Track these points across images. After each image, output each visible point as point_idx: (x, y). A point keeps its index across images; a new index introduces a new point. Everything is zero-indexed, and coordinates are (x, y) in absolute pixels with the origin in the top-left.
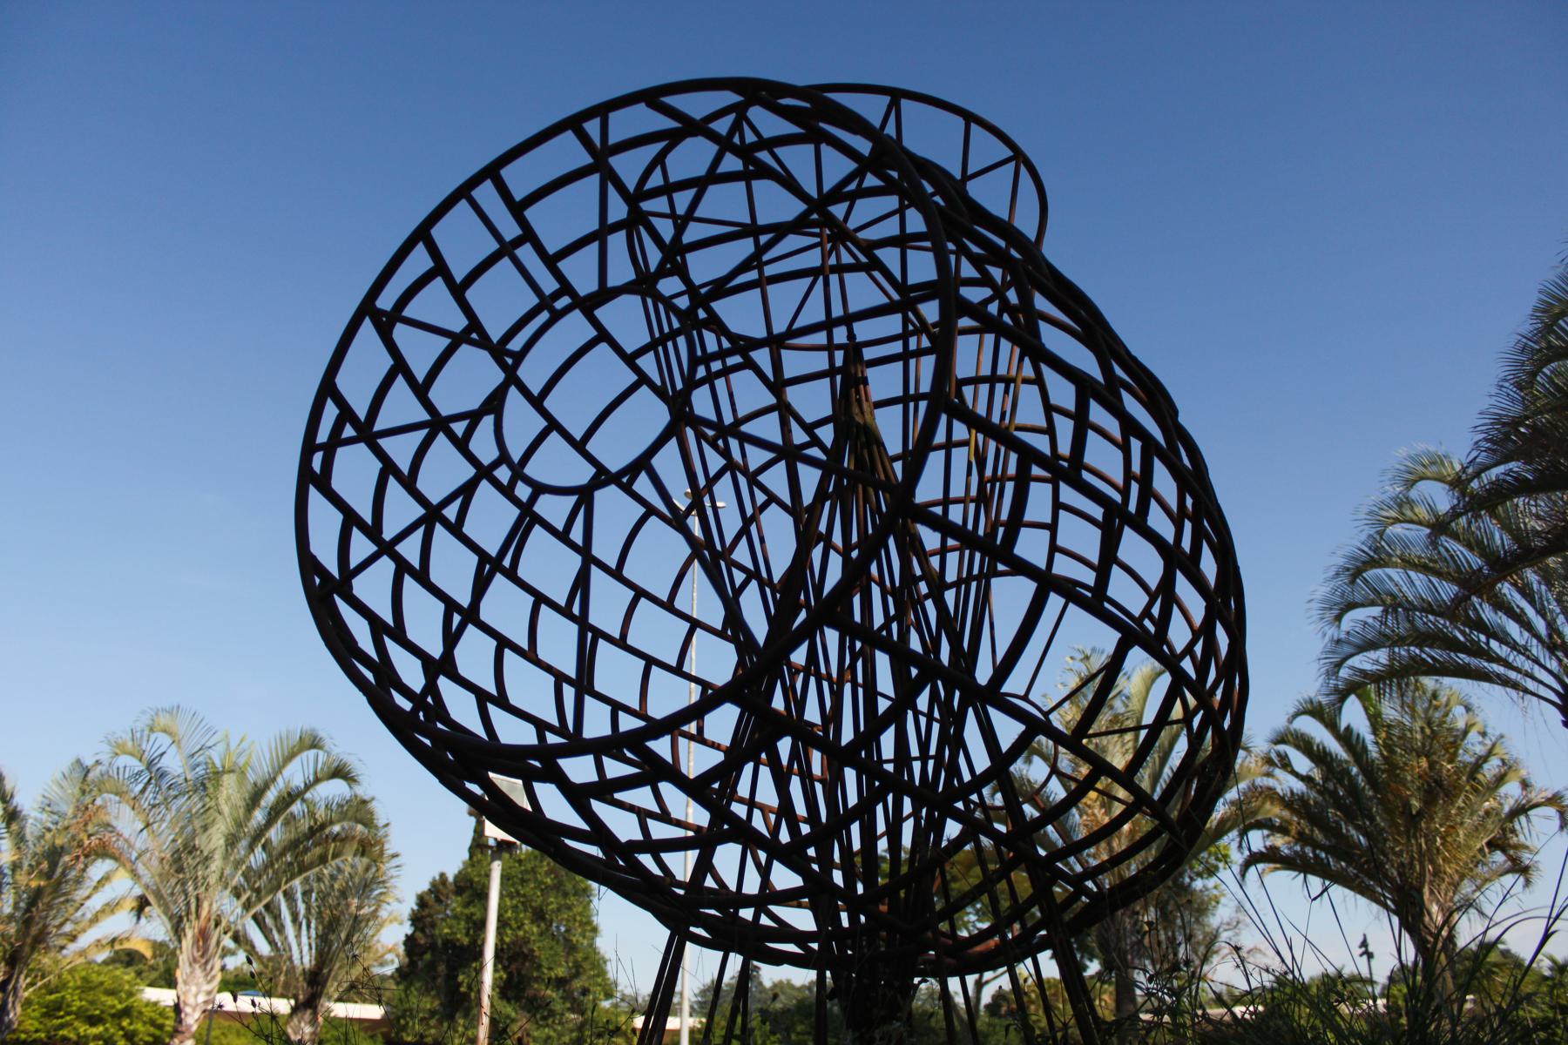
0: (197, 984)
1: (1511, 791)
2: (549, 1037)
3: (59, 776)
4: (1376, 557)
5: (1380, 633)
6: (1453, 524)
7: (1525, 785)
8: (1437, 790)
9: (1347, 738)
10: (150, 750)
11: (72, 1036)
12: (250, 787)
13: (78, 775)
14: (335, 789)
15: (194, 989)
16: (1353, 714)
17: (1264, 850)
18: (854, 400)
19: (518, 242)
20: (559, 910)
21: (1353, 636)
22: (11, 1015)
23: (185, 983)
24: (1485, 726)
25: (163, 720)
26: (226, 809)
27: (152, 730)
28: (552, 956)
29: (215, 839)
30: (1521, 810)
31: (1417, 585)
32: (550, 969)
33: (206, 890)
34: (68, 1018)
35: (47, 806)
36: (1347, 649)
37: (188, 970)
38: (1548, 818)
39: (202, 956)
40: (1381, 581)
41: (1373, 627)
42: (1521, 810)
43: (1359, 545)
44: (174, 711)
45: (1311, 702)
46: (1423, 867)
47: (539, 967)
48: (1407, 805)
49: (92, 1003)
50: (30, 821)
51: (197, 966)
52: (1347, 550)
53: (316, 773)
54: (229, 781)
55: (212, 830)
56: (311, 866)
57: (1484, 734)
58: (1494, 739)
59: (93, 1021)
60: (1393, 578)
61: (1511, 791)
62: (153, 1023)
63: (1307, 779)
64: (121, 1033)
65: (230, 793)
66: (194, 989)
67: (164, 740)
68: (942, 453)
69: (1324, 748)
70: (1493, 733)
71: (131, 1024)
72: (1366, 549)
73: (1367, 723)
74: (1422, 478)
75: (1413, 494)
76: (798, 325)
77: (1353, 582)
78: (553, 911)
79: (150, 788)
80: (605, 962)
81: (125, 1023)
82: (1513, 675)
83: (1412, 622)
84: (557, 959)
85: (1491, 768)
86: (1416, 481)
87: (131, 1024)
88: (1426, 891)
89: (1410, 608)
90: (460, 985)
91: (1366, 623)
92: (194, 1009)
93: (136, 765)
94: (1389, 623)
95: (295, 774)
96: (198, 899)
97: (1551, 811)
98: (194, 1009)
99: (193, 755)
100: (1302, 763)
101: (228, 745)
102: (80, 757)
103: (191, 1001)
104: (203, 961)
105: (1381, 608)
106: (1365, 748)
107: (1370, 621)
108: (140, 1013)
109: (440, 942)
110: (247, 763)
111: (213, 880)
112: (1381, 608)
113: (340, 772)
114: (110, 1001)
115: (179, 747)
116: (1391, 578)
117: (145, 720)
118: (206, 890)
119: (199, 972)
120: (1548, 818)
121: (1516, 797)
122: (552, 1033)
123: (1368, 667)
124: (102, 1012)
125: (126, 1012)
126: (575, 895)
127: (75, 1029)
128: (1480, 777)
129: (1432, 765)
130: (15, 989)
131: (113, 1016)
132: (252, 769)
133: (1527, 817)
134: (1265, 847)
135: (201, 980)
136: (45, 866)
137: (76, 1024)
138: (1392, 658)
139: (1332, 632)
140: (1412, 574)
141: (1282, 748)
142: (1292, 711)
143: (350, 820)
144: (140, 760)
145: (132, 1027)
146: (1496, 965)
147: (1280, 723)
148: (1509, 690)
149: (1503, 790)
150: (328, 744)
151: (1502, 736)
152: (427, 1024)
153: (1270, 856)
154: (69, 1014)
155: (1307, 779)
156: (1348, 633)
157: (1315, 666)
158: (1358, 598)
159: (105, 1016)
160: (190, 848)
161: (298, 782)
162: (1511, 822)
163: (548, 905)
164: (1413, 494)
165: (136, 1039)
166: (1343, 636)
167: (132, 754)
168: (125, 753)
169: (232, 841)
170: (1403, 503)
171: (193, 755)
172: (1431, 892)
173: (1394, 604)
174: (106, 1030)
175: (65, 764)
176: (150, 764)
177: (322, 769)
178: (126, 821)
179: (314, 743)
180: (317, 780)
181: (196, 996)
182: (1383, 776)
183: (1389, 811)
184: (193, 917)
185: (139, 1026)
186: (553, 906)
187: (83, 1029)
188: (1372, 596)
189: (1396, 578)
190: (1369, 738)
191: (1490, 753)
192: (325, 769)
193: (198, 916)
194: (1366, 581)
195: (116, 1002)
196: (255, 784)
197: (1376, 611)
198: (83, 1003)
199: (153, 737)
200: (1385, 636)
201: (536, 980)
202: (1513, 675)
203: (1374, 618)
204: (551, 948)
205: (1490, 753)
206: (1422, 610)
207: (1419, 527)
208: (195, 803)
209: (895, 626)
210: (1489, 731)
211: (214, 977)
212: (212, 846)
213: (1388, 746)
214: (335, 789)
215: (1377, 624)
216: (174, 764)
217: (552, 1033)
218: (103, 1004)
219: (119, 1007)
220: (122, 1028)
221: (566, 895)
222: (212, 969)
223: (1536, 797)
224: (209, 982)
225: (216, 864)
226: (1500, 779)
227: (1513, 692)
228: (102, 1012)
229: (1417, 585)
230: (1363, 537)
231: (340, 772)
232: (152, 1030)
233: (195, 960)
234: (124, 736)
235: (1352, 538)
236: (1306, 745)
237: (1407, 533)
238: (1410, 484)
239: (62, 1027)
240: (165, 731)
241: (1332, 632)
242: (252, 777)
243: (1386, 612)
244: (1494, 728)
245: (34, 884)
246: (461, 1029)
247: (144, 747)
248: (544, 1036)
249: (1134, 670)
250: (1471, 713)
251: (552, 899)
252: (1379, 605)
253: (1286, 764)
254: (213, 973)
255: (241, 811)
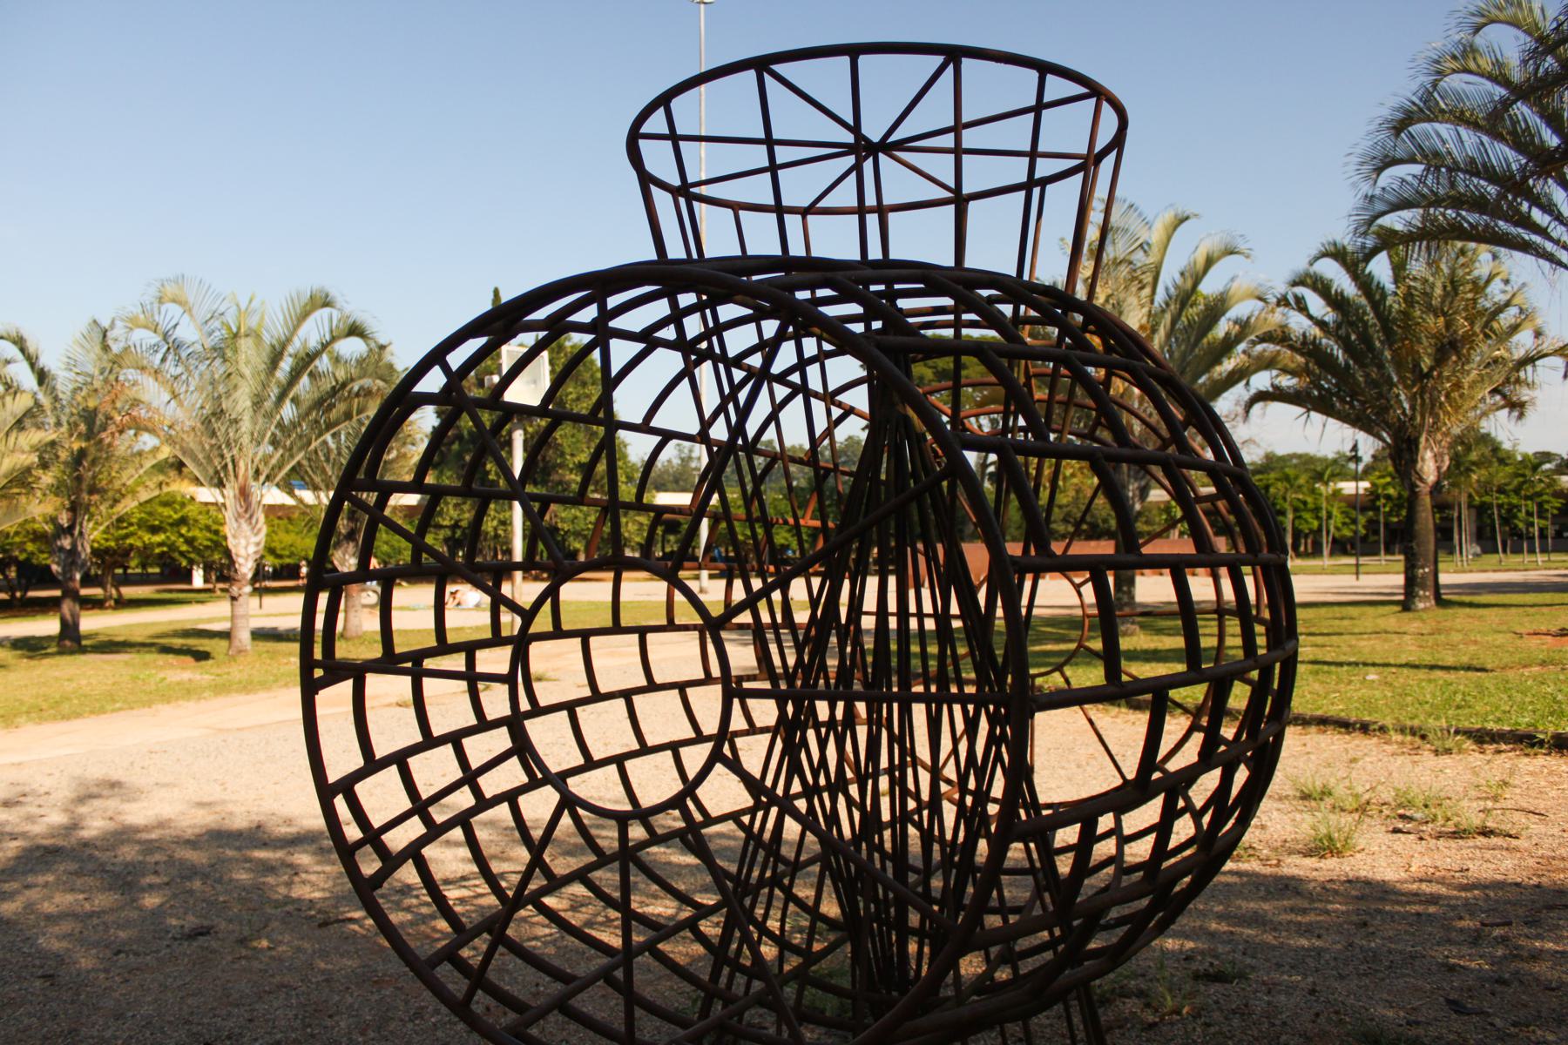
0: (246, 537)
1: (1523, 342)
2: (576, 517)
3: (78, 335)
4: (1425, 109)
5: (1417, 192)
6: (1524, 161)
7: (1538, 334)
8: (1450, 347)
9: (1366, 284)
10: (165, 325)
11: (139, 544)
12: (268, 349)
13: (98, 337)
14: (351, 348)
15: (243, 542)
16: (1380, 268)
17: (1271, 389)
18: (905, 999)
19: (477, 792)
20: (578, 399)
21: (1389, 193)
22: (83, 556)
23: (234, 537)
24: (1510, 274)
25: (170, 290)
26: (247, 372)
27: (161, 301)
28: (574, 443)
29: (241, 402)
30: (1529, 360)
31: (1463, 142)
32: (572, 455)
33: (240, 449)
34: (132, 529)
35: (71, 364)
36: (1380, 207)
37: (235, 525)
38: (1554, 369)
39: (246, 511)
40: (1428, 137)
41: (1411, 185)
42: (1529, 360)
43: (1409, 95)
44: (179, 280)
45: (1335, 244)
46: (1423, 418)
47: (562, 454)
48: (1417, 365)
49: (150, 514)
50: (60, 380)
51: (242, 521)
52: (1395, 102)
53: (331, 331)
54: (245, 344)
55: (237, 395)
56: (337, 423)
57: (1507, 282)
58: (1516, 288)
59: (154, 530)
60: (1442, 135)
61: (1523, 342)
62: (208, 528)
63: (1321, 324)
64: (181, 540)
65: (250, 358)
66: (243, 542)
67: (173, 311)
68: (653, 820)
69: (1342, 293)
70: (1516, 281)
71: (189, 531)
72: (1417, 102)
73: (1390, 273)
74: (1493, 21)
75: (1479, 40)
76: (822, 204)
77: (1397, 135)
78: (573, 400)
79: (170, 357)
80: (625, 446)
81: (184, 530)
82: (1549, 246)
83: (1453, 185)
84: (579, 445)
85: (1507, 318)
86: (1485, 25)
87: (189, 531)
88: (1422, 440)
89: (1454, 168)
90: (488, 473)
91: (1403, 180)
92: (247, 559)
93: (155, 339)
94: (1429, 182)
95: (312, 333)
96: (233, 461)
97: (1559, 362)
98: (247, 559)
99: (206, 322)
100: (1316, 304)
101: (238, 305)
102: (96, 318)
103: (242, 552)
104: (247, 516)
105: (1422, 167)
106: (1384, 296)
107: (1409, 179)
108: (196, 521)
109: (465, 433)
110: (260, 324)
111: (246, 440)
112: (1422, 167)
113: (355, 330)
114: (166, 512)
115: (191, 316)
116: (1439, 135)
117: (153, 292)
118: (240, 449)
119: (245, 526)
120: (1554, 369)
121: (1527, 347)
122: (578, 514)
123: (1399, 227)
124: (161, 522)
125: (183, 521)
126: (593, 384)
127: (140, 538)
128: (1495, 325)
129: (1448, 325)
130: (81, 533)
131: (172, 525)
132: (267, 331)
133: (1534, 366)
134: (1272, 385)
135: (249, 533)
136: (83, 427)
137: (140, 533)
138: (1424, 218)
139: (1366, 188)
140: (1461, 130)
141: (1300, 290)
142: (1314, 252)
143: (370, 376)
144: (155, 332)
145: (190, 534)
146: (1474, 463)
147: (1300, 265)
148: (1541, 261)
149: (1516, 338)
150: (339, 301)
151: (1524, 285)
152: (462, 510)
153: (1276, 395)
154: (131, 524)
155: (1321, 324)
156: (1383, 189)
157: (1345, 223)
158: (1400, 153)
159: (164, 525)
160: (219, 413)
161: (313, 343)
162: (1518, 371)
163: (567, 395)
164: (1479, 40)
165: (196, 544)
166: (1378, 192)
167: (146, 327)
168: (139, 327)
169: (258, 403)
170: (1469, 50)
171: (206, 322)
172: (1427, 440)
173: (1434, 159)
174: (168, 538)
175: (82, 325)
176: (165, 336)
177: (337, 327)
178: (153, 393)
179: (327, 303)
180: (334, 339)
181: (246, 548)
182: (1396, 328)
183: (1399, 364)
184: (232, 478)
185: (195, 533)
186: (573, 396)
187: (147, 537)
188: (1419, 157)
189: (1445, 135)
190: (1390, 287)
191: (1508, 304)
192: (341, 326)
193: (236, 476)
194: (1411, 137)
195: (172, 513)
196: (273, 347)
197: (1417, 169)
198: (143, 515)
199: (163, 308)
200: (1423, 196)
201: (561, 466)
202: (1549, 246)
203: (1414, 176)
204: (573, 436)
205: (1508, 304)
206: (1465, 172)
207: (1483, 81)
208: (219, 368)
209: (925, 813)
210: (1513, 278)
211: (260, 530)
212: (239, 408)
213: (1409, 298)
214: (351, 348)
215: (1416, 183)
216: (188, 333)
217: (578, 514)
218: (161, 515)
219: (176, 516)
220: (182, 535)
221: (584, 384)
222: (257, 522)
223: (1547, 346)
224: (256, 534)
225: (246, 425)
226: (1515, 328)
227: (1545, 265)
228: (161, 522)
229: (1463, 142)
230: (1414, 86)
231: (355, 330)
232: (208, 535)
233: (239, 515)
234: (135, 311)
235: (1404, 88)
236: (1322, 287)
237: (1464, 86)
238: (1477, 29)
239: (127, 536)
240: (174, 301)
241: (1366, 188)
242: (267, 338)
243: (1427, 170)
244: (1518, 276)
245: (76, 447)
246: (492, 513)
247: (156, 318)
248: (570, 516)
249: (1156, 217)
250: (1497, 262)
251: (570, 390)
252: (1421, 163)
253: (1301, 306)
254: (258, 526)
255: (263, 376)
